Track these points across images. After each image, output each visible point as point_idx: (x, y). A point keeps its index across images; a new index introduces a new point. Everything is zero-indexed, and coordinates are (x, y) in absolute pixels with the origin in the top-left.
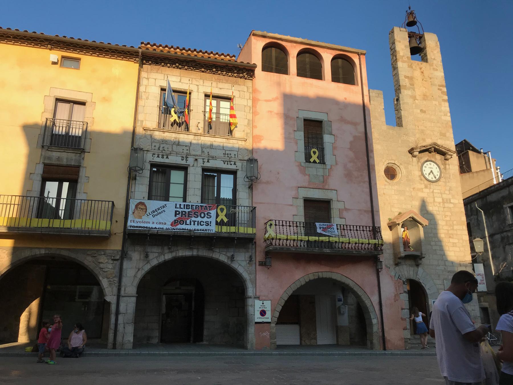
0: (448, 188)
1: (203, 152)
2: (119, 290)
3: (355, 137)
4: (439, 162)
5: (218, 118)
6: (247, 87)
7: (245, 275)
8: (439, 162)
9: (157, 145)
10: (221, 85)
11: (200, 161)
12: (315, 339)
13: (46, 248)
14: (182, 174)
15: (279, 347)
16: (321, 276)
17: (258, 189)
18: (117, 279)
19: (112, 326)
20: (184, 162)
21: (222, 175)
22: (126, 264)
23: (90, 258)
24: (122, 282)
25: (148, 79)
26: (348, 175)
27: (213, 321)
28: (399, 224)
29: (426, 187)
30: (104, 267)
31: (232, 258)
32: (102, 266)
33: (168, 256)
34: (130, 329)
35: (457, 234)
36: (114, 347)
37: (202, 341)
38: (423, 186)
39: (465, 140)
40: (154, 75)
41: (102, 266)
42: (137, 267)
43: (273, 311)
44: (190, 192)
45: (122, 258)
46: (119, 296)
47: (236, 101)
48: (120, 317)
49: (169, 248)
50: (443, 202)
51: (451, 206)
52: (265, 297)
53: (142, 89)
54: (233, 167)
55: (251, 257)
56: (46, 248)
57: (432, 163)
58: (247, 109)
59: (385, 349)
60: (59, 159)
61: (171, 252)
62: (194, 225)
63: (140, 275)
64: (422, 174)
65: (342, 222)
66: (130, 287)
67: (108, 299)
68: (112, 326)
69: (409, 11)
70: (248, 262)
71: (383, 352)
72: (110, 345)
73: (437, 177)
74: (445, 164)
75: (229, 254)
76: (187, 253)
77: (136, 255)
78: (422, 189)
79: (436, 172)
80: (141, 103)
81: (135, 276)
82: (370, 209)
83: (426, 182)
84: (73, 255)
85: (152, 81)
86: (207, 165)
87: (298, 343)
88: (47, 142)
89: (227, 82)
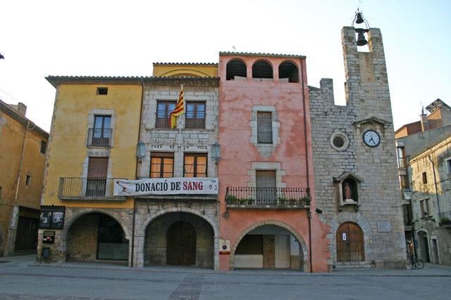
0: (385, 151)
1: (184, 141)
2: (133, 232)
3: (296, 122)
4: (378, 131)
5: (195, 115)
6: (152, 130)
7: (213, 224)
8: (378, 131)
9: (155, 140)
10: (196, 93)
11: (182, 148)
12: (274, 264)
13: (92, 208)
14: (61, 214)
15: (235, 269)
16: (266, 223)
17: (222, 163)
18: (132, 226)
19: (130, 254)
20: (171, 150)
21: (198, 158)
22: (137, 216)
23: (116, 214)
24: (135, 226)
25: (149, 95)
26: (290, 152)
27: (147, 262)
28: (340, 181)
29: (367, 151)
30: (124, 219)
31: (204, 213)
32: (123, 218)
33: (163, 212)
34: (141, 256)
35: (391, 187)
36: (132, 266)
37: (195, 264)
38: (364, 151)
39: (438, 100)
40: (152, 92)
41: (123, 218)
42: (144, 217)
43: (232, 246)
44: (176, 169)
45: (134, 213)
46: (133, 236)
47: (207, 104)
48: (135, 249)
49: (163, 207)
50: (381, 163)
51: (388, 164)
52: (226, 237)
53: (145, 102)
54: (205, 151)
55: (216, 212)
56: (92, 208)
57: (373, 132)
58: (215, 108)
59: (311, 272)
60: (97, 153)
61: (164, 209)
62: (190, 183)
63: (146, 223)
64: (364, 141)
65: (284, 185)
66: (140, 230)
67: (127, 237)
68: (130, 254)
69: (358, 12)
70: (65, 258)
71: (310, 274)
72: (130, 265)
73: (376, 143)
74: (384, 132)
75: (202, 210)
76: (175, 210)
77: (142, 210)
78: (363, 153)
79: (376, 139)
80: (144, 112)
81: (143, 224)
82: (306, 175)
83: (367, 147)
84: (106, 212)
85: (151, 96)
86: (187, 150)
87: (262, 266)
88: (90, 143)
89: (201, 91)
